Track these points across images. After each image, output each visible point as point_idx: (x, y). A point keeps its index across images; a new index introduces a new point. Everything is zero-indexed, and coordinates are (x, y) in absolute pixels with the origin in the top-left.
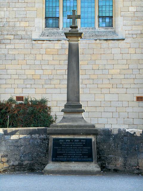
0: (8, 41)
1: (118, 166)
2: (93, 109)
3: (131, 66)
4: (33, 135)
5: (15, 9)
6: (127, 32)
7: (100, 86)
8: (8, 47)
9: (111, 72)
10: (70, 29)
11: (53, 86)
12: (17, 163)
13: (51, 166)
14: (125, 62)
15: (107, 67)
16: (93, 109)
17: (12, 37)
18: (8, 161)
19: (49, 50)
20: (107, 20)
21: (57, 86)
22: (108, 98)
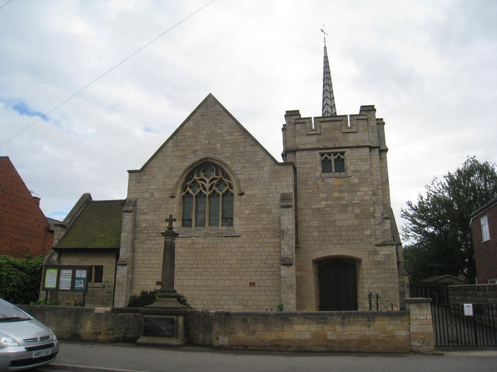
0: (153, 238)
1: (199, 340)
2: (215, 293)
3: (245, 258)
4: (136, 314)
5: (159, 213)
6: (242, 230)
7: (221, 273)
8: (152, 242)
9: (230, 262)
10: (167, 229)
11: (184, 273)
12: (121, 335)
13: (142, 339)
14: (241, 253)
15: (227, 258)
16: (215, 293)
17: (156, 235)
18: (113, 334)
19: (183, 244)
20: (229, 220)
21: (187, 273)
22: (227, 283)
